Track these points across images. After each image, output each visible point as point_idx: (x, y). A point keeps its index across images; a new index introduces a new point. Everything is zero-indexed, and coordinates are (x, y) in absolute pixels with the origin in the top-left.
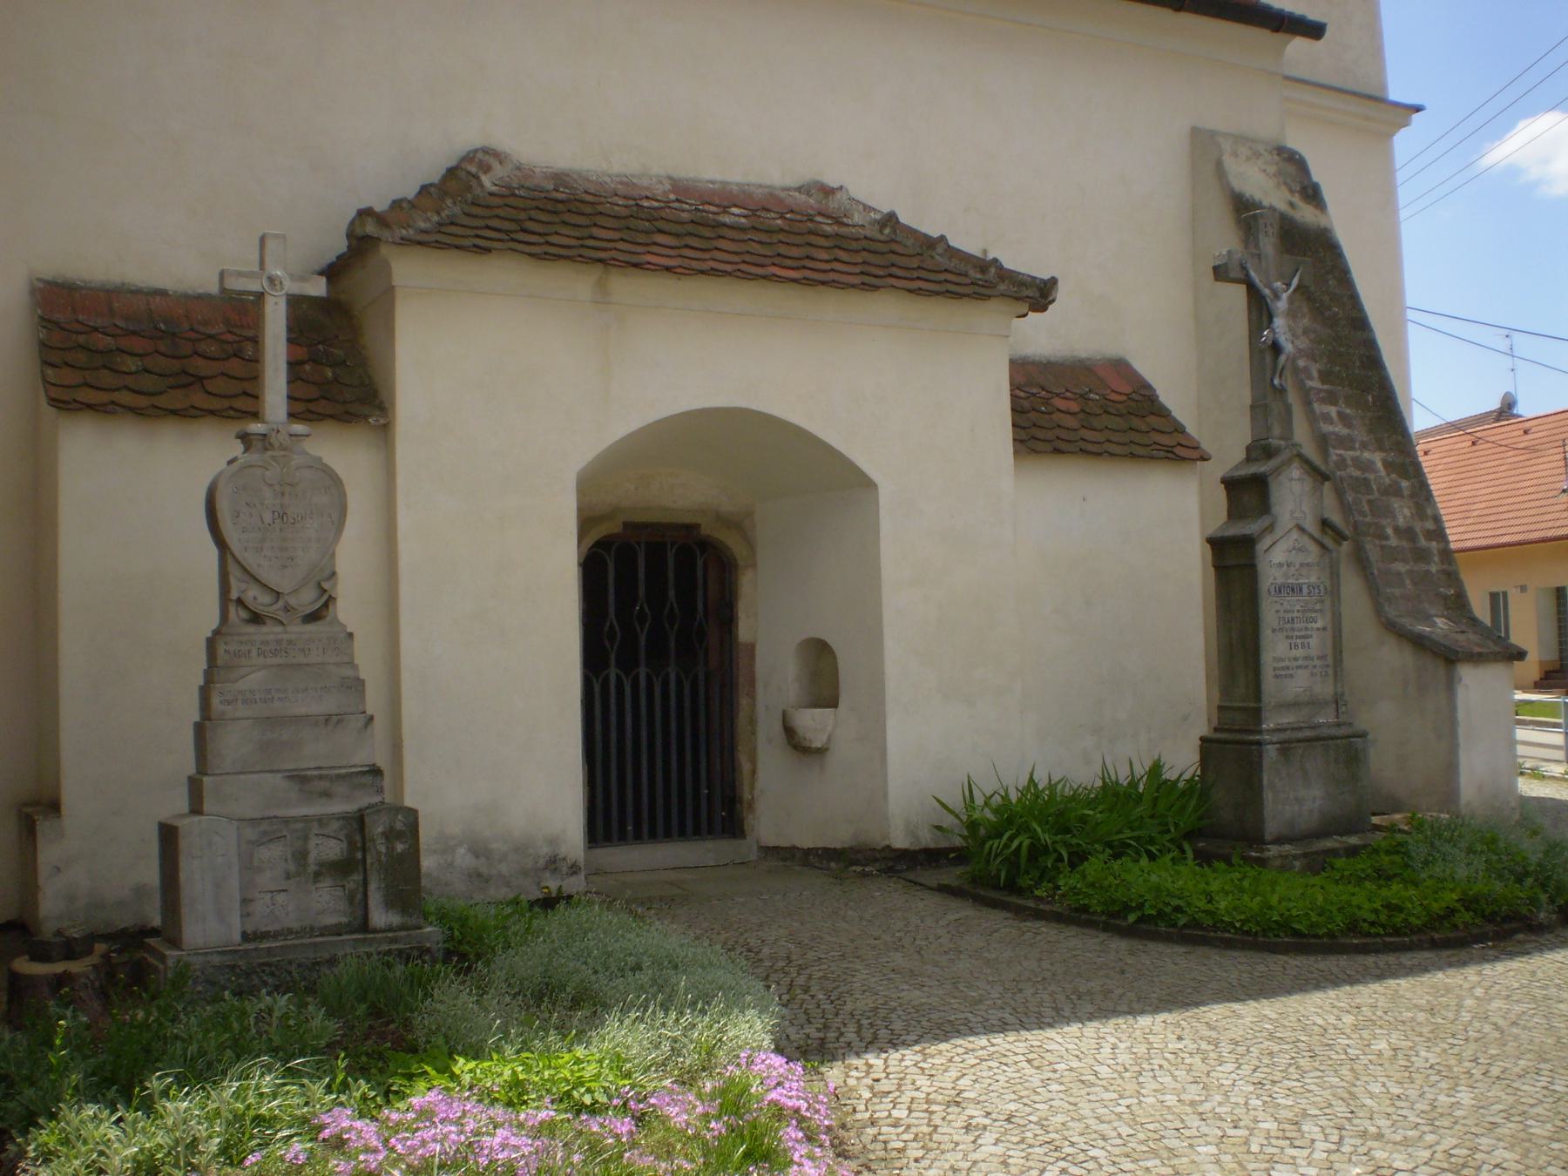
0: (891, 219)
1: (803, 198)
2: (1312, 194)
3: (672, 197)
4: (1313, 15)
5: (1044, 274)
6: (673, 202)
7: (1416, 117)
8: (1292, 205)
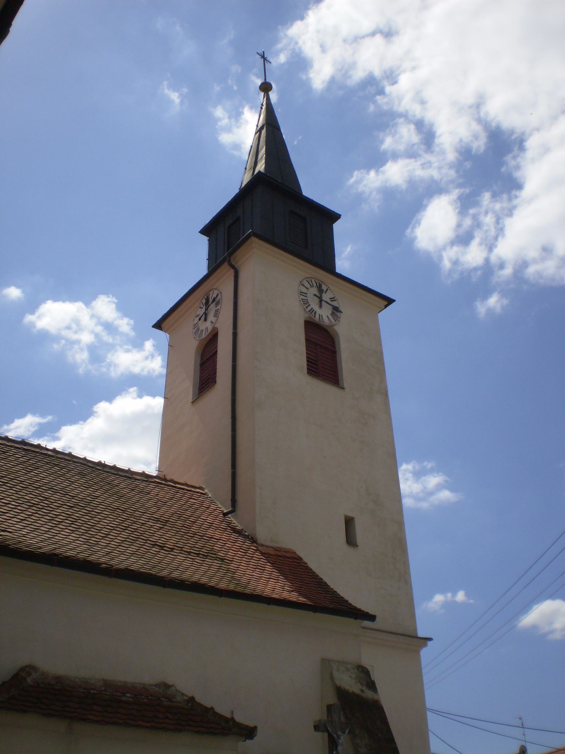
0: (192, 699)
1: (157, 689)
2: (372, 686)
3: (103, 688)
4: (371, 612)
5: (252, 724)
6: (103, 691)
7: (429, 643)
8: (362, 691)
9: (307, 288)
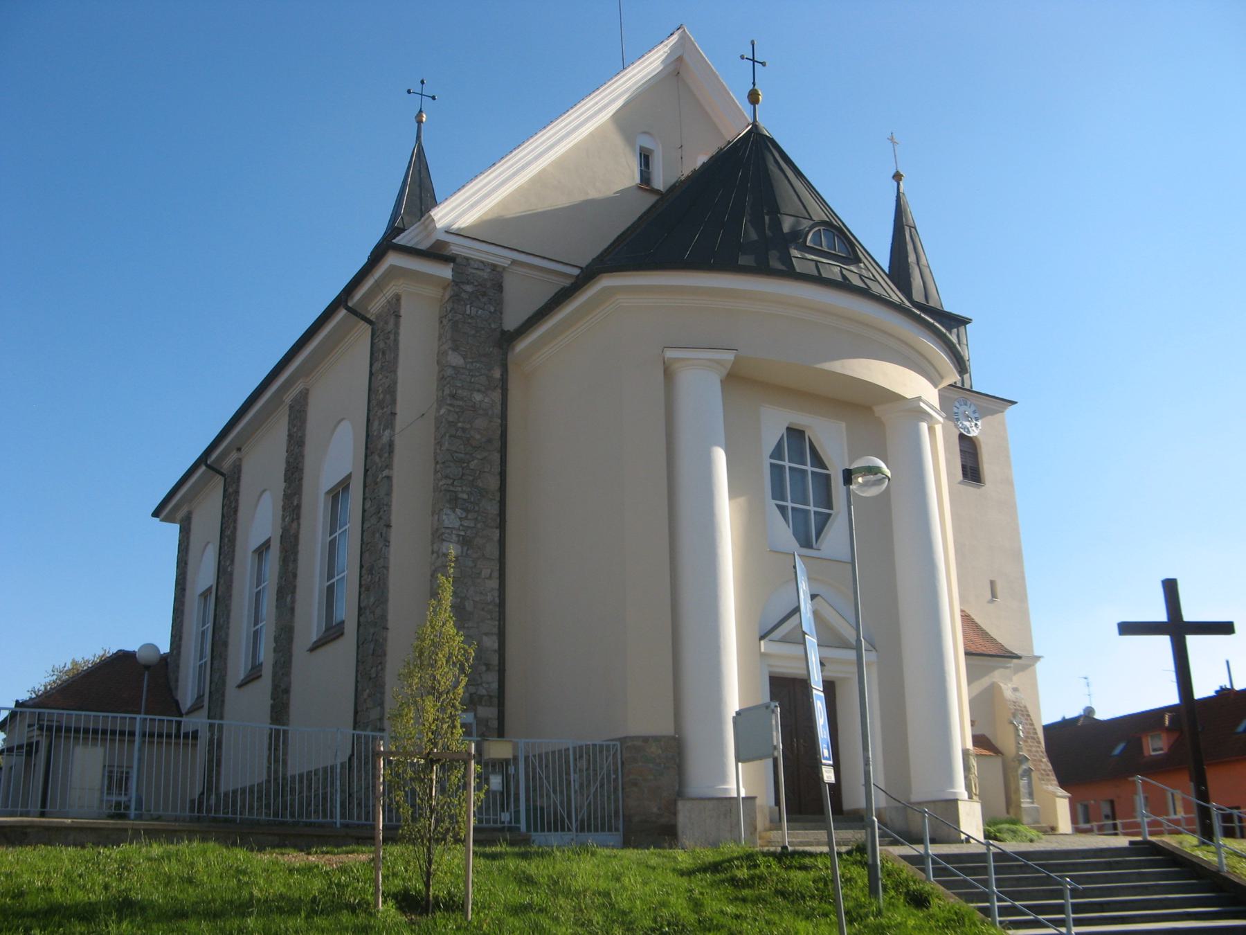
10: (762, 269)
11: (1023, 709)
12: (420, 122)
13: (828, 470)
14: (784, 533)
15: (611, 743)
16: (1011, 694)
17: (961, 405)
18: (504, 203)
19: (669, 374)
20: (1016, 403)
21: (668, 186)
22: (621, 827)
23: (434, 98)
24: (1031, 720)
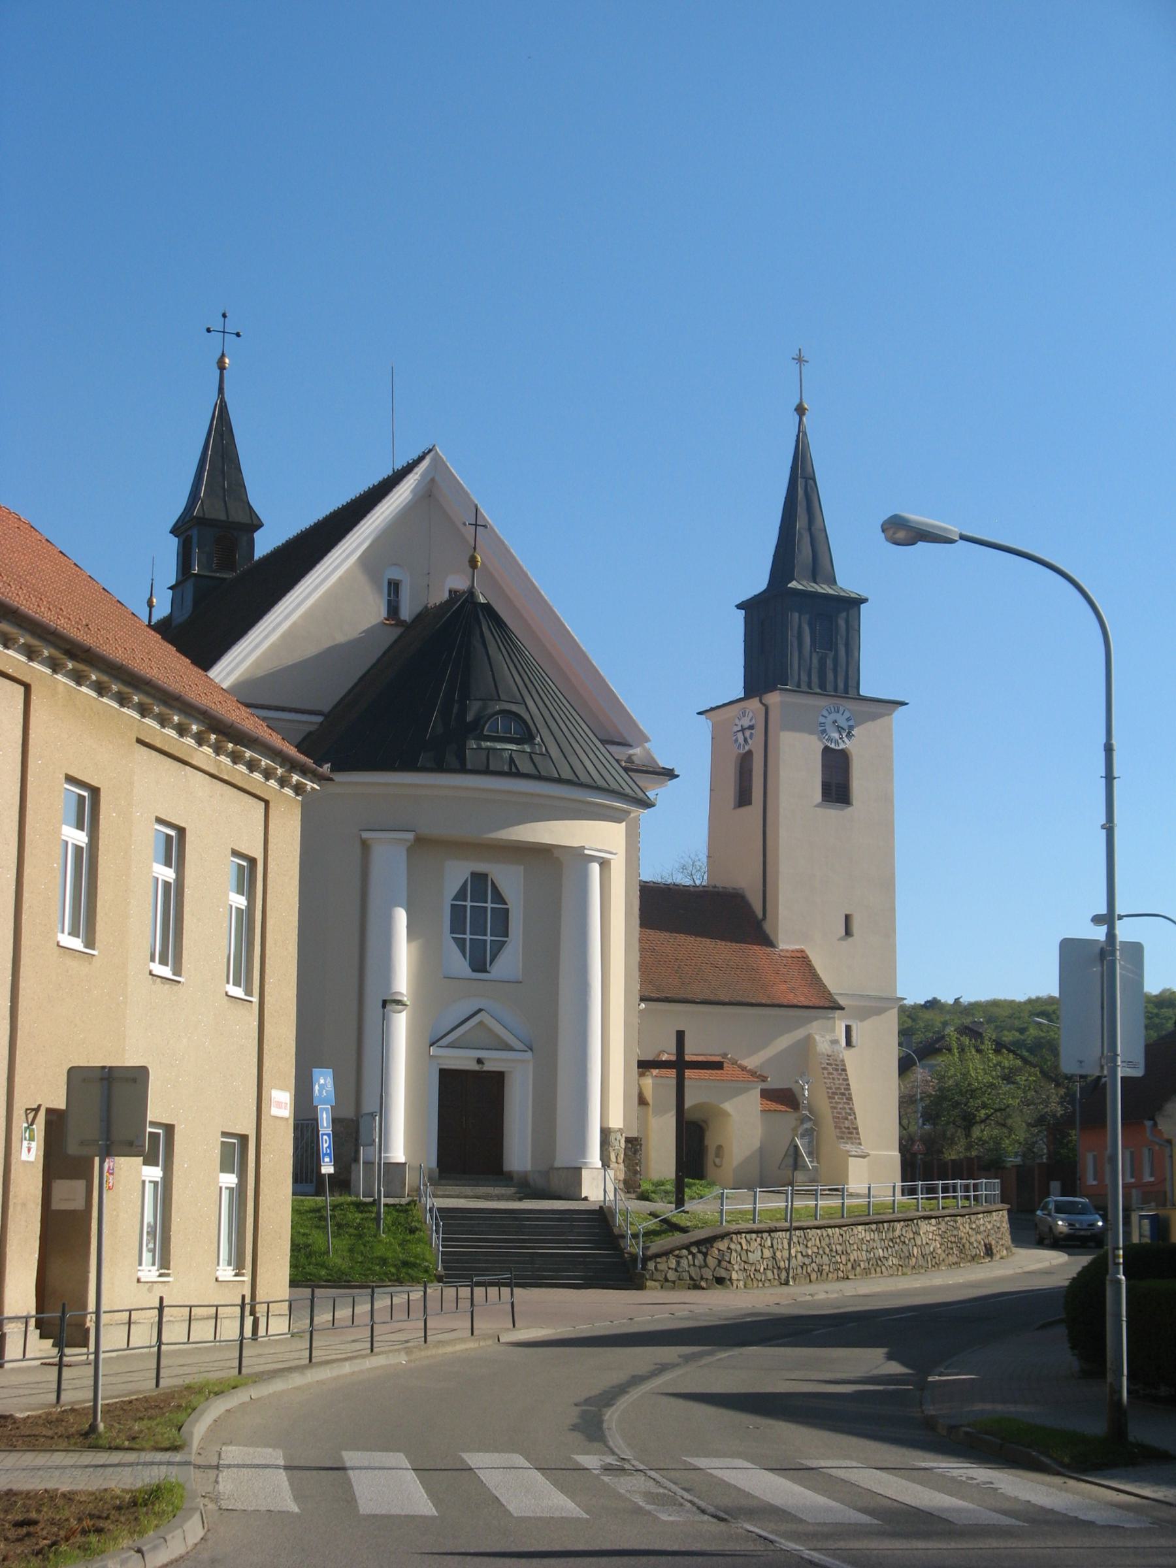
9: (826, 717)
10: (440, 767)
11: (838, 1063)
12: (222, 367)
13: (453, 938)
14: (460, 965)
15: (310, 1122)
16: (828, 1048)
17: (830, 713)
18: (257, 663)
19: (365, 846)
20: (907, 704)
21: (413, 616)
22: (314, 1180)
23: (238, 335)
24: (847, 1075)
